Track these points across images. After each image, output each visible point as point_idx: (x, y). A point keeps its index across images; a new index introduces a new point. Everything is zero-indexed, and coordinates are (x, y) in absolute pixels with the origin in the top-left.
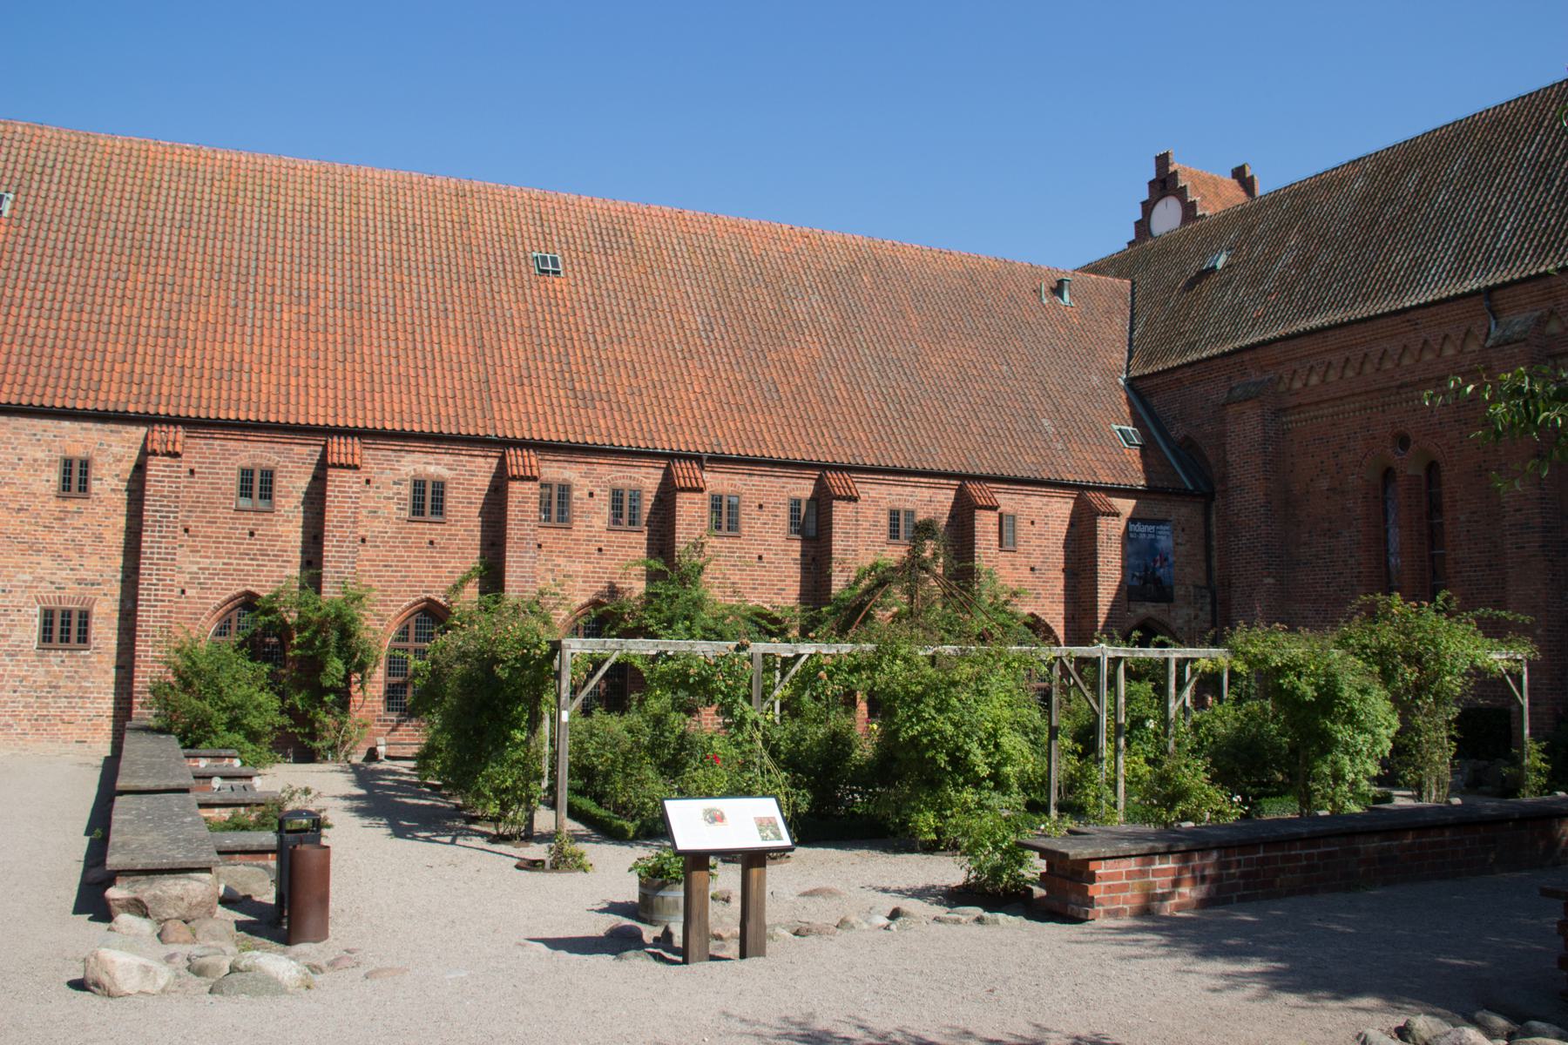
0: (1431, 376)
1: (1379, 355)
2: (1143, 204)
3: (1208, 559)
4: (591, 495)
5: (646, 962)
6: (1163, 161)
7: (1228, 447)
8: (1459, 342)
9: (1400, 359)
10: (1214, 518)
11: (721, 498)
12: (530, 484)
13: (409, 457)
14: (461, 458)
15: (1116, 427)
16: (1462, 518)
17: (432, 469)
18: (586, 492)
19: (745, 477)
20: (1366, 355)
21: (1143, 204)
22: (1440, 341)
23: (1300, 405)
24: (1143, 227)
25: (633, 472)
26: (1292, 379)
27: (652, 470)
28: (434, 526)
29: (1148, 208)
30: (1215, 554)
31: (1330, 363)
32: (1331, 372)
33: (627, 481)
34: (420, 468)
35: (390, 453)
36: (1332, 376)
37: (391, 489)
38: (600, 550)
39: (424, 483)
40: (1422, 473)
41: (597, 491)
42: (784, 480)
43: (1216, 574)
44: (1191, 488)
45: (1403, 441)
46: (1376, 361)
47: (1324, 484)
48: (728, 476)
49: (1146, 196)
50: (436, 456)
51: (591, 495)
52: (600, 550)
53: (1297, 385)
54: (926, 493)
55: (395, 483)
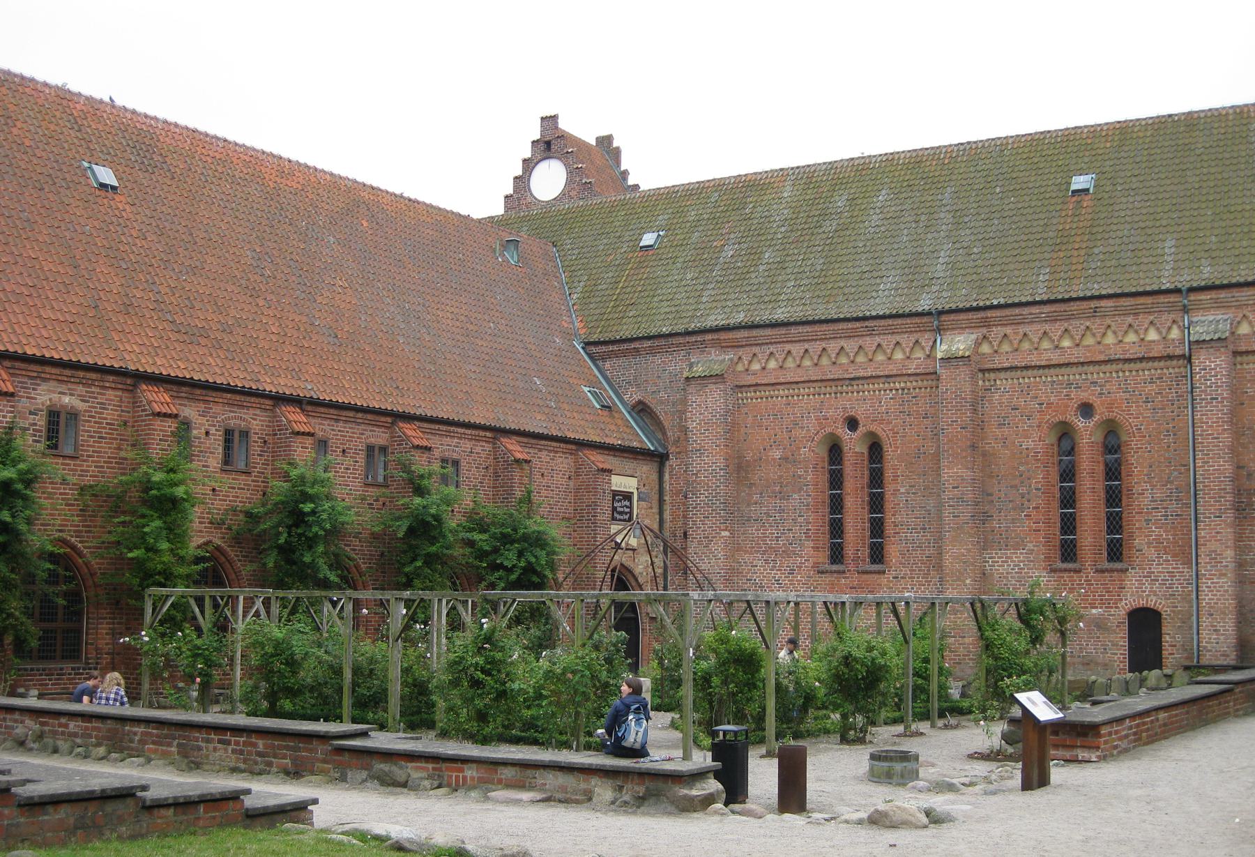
0: (882, 374)
1: (837, 351)
2: (525, 161)
3: (661, 513)
4: (207, 433)
5: (868, 787)
6: (550, 121)
7: (689, 415)
8: (908, 350)
9: (855, 356)
10: (667, 477)
11: (58, 414)
12: (169, 422)
13: (44, 387)
14: (93, 389)
15: (586, 389)
16: (902, 490)
17: (66, 400)
18: (203, 431)
19: (333, 423)
20: (824, 349)
21: (525, 161)
22: (892, 346)
23: (757, 385)
24: (522, 182)
25: (243, 413)
26: (750, 362)
27: (258, 412)
28: (68, 461)
29: (529, 165)
30: (667, 508)
31: (789, 352)
32: (790, 359)
33: (238, 422)
34: (55, 396)
35: (26, 380)
36: (790, 363)
37: (26, 419)
38: (214, 490)
39: (58, 414)
40: (865, 451)
41: (213, 430)
42: (363, 427)
43: (667, 525)
44: (652, 448)
45: (852, 423)
46: (834, 355)
47: (777, 454)
48: (319, 420)
49: (528, 154)
50: (70, 386)
51: (207, 433)
52: (214, 490)
53: (756, 367)
54: (468, 445)
55: (31, 413)
